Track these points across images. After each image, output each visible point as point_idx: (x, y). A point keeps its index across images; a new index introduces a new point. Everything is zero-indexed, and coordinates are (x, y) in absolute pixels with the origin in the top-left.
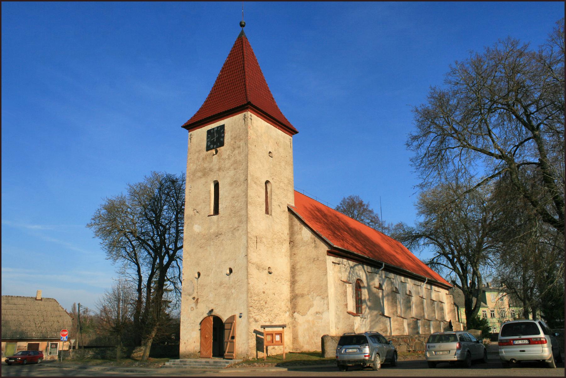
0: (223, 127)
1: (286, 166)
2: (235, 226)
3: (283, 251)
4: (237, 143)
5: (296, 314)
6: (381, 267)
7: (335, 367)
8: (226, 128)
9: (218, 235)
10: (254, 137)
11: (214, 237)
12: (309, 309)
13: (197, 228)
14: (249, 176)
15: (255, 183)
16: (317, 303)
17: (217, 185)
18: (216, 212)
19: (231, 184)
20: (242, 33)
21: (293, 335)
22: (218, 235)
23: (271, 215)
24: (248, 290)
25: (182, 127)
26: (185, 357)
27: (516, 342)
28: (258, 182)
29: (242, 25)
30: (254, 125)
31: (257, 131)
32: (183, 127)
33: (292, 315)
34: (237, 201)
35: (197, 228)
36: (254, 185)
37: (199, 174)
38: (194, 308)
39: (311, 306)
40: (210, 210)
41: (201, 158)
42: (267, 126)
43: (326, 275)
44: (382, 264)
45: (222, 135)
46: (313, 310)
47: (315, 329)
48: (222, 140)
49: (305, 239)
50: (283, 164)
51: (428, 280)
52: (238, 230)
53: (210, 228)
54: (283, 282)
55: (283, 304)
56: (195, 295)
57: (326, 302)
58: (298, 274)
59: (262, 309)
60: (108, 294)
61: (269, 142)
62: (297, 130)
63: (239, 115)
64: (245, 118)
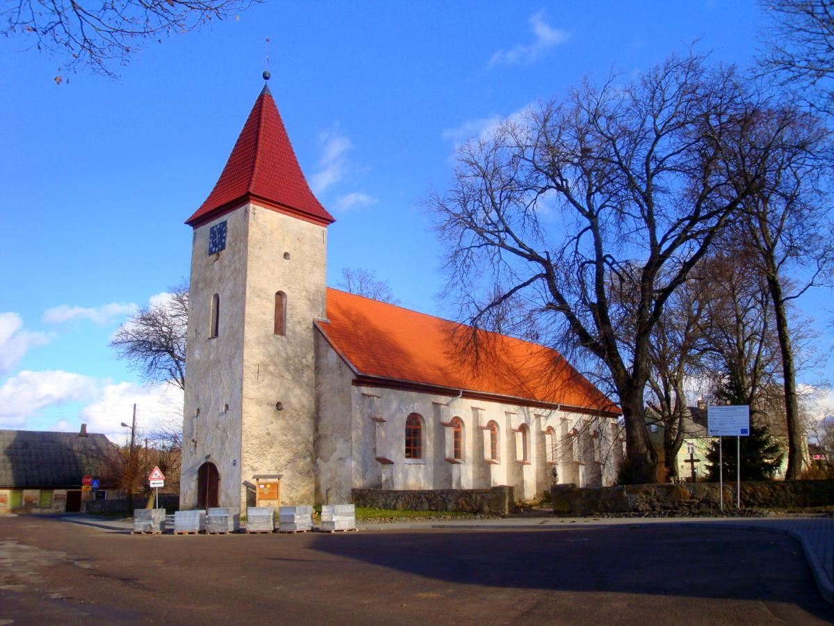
0: (225, 224)
1: (314, 269)
4: (238, 245)
5: (318, 460)
6: (459, 395)
7: (550, 513)
8: (228, 226)
10: (259, 237)
12: (332, 454)
14: (248, 288)
15: (258, 296)
16: (340, 445)
18: (216, 334)
20: (265, 88)
21: (316, 486)
25: (186, 223)
29: (266, 78)
30: (260, 221)
31: (265, 227)
32: (187, 223)
33: (315, 461)
36: (257, 300)
39: (334, 450)
40: (208, 333)
43: (350, 411)
44: (459, 391)
45: (224, 235)
46: (335, 456)
47: (337, 480)
48: (223, 241)
49: (331, 364)
50: (308, 266)
51: (561, 406)
56: (194, 437)
57: (349, 445)
58: (323, 408)
59: (264, 454)
60: (248, 415)
61: (284, 240)
62: (335, 217)
64: (247, 212)
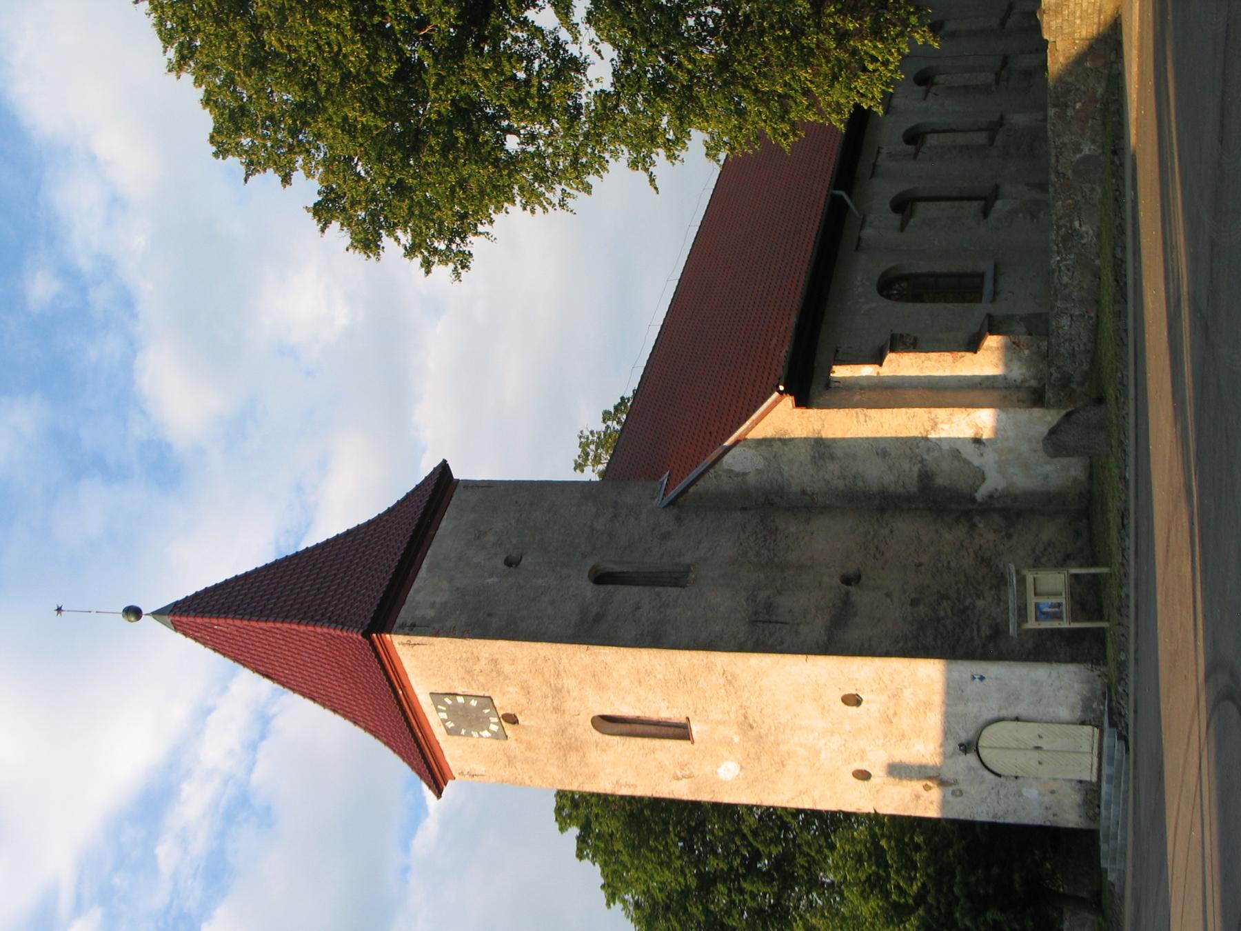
2: (722, 681)
3: (793, 529)
9: (747, 725)
11: (752, 733)
13: (728, 770)
17: (609, 723)
18: (680, 731)
19: (601, 687)
20: (158, 614)
22: (747, 725)
23: (689, 566)
24: (875, 165)
26: (1095, 817)
27: (1196, 723)
28: (595, 610)
34: (649, 673)
35: (728, 770)
37: (573, 758)
38: (954, 787)
41: (528, 754)
42: (429, 570)
52: (733, 676)
53: (729, 743)
54: (886, 531)
55: (948, 536)
63: (402, 658)
